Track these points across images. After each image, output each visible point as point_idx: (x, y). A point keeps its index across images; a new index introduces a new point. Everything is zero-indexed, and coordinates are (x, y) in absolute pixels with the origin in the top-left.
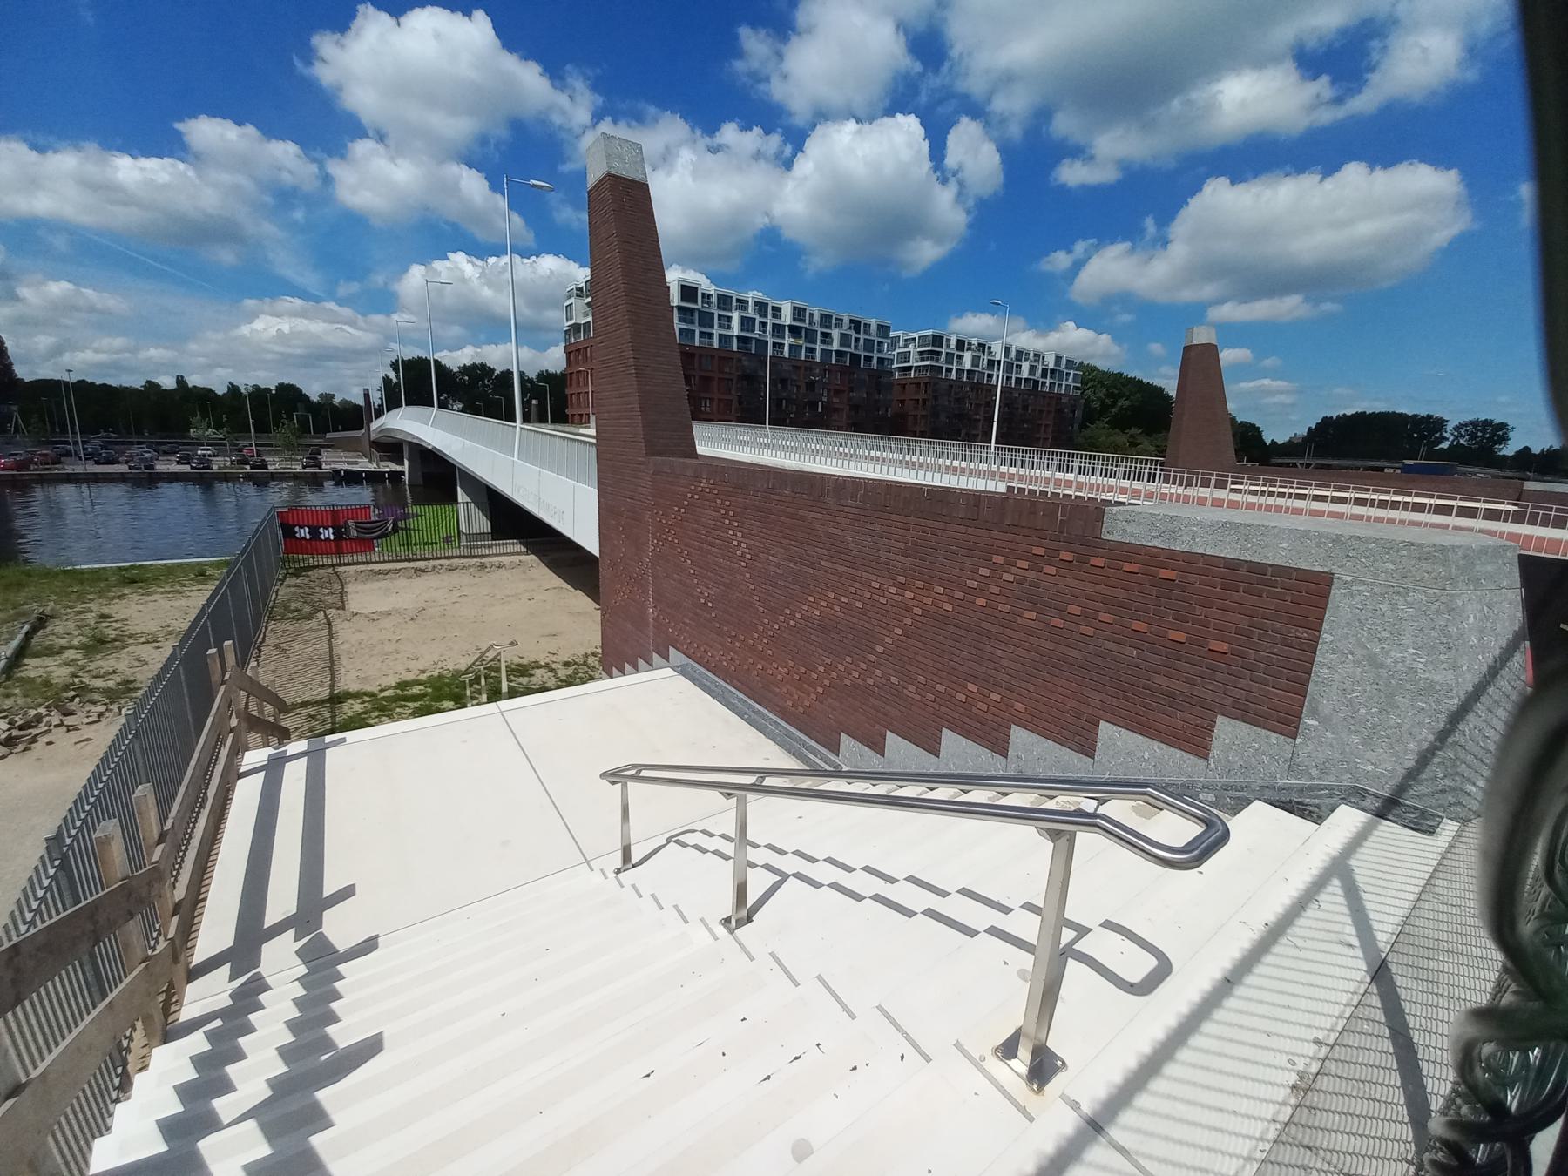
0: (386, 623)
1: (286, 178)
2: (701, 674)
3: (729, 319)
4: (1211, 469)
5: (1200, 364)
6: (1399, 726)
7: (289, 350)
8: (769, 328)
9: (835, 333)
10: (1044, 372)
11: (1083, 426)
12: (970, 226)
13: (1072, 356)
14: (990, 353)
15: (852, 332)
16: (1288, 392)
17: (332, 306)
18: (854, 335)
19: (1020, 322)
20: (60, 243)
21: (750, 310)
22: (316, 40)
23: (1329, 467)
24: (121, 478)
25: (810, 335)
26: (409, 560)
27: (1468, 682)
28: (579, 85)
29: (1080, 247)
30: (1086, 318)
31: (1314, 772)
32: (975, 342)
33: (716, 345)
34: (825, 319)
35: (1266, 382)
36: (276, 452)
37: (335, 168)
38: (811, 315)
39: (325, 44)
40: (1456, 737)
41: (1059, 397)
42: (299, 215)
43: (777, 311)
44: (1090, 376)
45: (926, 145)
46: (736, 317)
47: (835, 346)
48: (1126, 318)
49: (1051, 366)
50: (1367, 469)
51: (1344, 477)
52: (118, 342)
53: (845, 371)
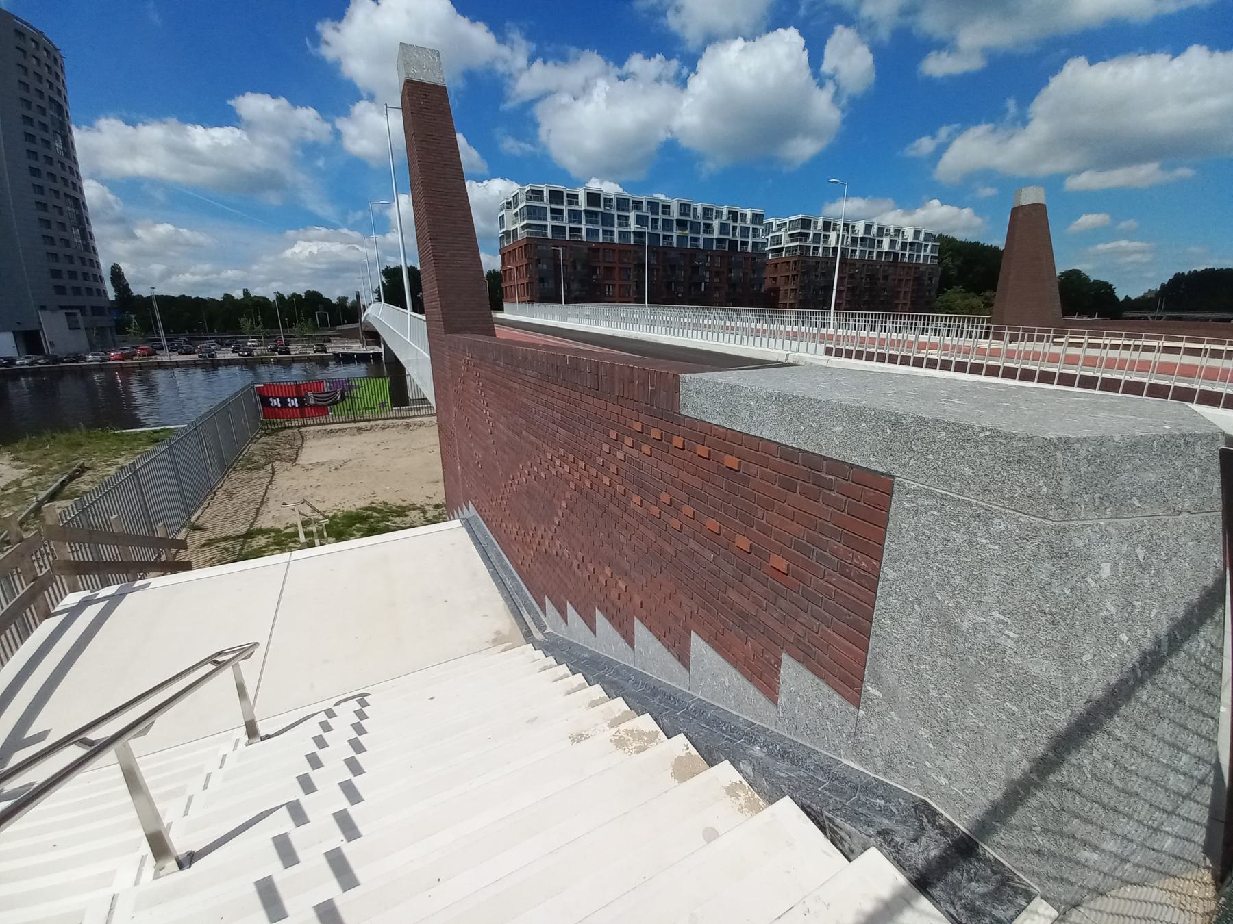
0: (316, 473)
1: (310, 136)
2: (480, 526)
3: (627, 218)
4: (1036, 324)
5: (1030, 223)
6: (980, 732)
7: (318, 266)
8: (660, 223)
9: (716, 224)
10: (904, 245)
11: (940, 291)
12: (844, 122)
13: (930, 230)
14: (853, 231)
15: (730, 222)
16: (1143, 252)
17: (345, 231)
18: (732, 224)
19: (889, 203)
20: (159, 195)
21: (644, 209)
22: (319, 27)
23: (1180, 319)
24: (195, 364)
25: (695, 227)
26: (355, 421)
27: (1095, 682)
28: (516, 36)
29: (943, 132)
30: (951, 196)
31: (880, 763)
32: (841, 222)
33: (550, 236)
34: (707, 212)
35: (1124, 243)
36: (296, 342)
37: (342, 124)
38: (695, 209)
39: (326, 30)
40: (1063, 775)
41: (917, 266)
42: (320, 163)
43: (666, 208)
44: (948, 246)
45: (805, 56)
46: (632, 216)
47: (716, 234)
48: (988, 192)
49: (910, 239)
50: (1169, 319)
51: (1196, 329)
52: (207, 267)
53: (724, 255)
